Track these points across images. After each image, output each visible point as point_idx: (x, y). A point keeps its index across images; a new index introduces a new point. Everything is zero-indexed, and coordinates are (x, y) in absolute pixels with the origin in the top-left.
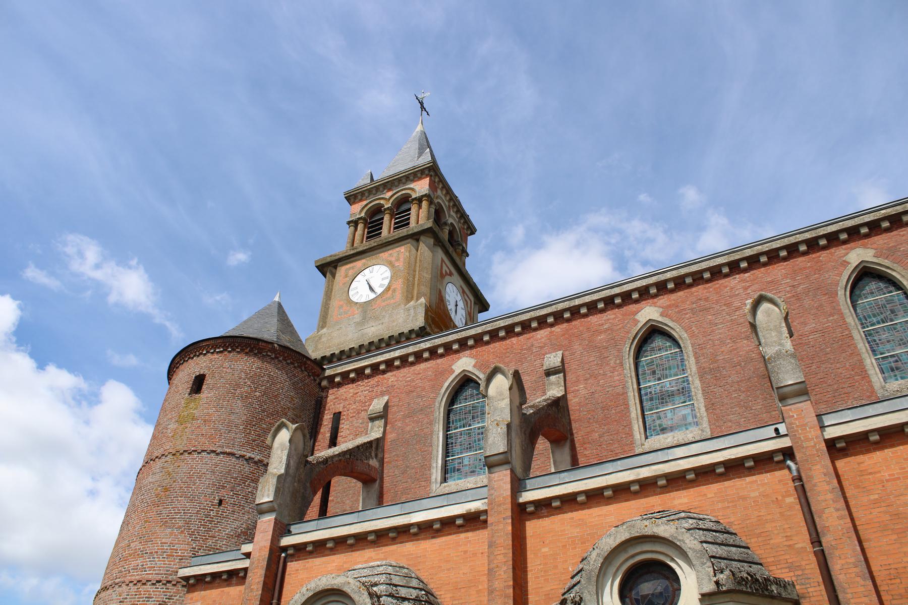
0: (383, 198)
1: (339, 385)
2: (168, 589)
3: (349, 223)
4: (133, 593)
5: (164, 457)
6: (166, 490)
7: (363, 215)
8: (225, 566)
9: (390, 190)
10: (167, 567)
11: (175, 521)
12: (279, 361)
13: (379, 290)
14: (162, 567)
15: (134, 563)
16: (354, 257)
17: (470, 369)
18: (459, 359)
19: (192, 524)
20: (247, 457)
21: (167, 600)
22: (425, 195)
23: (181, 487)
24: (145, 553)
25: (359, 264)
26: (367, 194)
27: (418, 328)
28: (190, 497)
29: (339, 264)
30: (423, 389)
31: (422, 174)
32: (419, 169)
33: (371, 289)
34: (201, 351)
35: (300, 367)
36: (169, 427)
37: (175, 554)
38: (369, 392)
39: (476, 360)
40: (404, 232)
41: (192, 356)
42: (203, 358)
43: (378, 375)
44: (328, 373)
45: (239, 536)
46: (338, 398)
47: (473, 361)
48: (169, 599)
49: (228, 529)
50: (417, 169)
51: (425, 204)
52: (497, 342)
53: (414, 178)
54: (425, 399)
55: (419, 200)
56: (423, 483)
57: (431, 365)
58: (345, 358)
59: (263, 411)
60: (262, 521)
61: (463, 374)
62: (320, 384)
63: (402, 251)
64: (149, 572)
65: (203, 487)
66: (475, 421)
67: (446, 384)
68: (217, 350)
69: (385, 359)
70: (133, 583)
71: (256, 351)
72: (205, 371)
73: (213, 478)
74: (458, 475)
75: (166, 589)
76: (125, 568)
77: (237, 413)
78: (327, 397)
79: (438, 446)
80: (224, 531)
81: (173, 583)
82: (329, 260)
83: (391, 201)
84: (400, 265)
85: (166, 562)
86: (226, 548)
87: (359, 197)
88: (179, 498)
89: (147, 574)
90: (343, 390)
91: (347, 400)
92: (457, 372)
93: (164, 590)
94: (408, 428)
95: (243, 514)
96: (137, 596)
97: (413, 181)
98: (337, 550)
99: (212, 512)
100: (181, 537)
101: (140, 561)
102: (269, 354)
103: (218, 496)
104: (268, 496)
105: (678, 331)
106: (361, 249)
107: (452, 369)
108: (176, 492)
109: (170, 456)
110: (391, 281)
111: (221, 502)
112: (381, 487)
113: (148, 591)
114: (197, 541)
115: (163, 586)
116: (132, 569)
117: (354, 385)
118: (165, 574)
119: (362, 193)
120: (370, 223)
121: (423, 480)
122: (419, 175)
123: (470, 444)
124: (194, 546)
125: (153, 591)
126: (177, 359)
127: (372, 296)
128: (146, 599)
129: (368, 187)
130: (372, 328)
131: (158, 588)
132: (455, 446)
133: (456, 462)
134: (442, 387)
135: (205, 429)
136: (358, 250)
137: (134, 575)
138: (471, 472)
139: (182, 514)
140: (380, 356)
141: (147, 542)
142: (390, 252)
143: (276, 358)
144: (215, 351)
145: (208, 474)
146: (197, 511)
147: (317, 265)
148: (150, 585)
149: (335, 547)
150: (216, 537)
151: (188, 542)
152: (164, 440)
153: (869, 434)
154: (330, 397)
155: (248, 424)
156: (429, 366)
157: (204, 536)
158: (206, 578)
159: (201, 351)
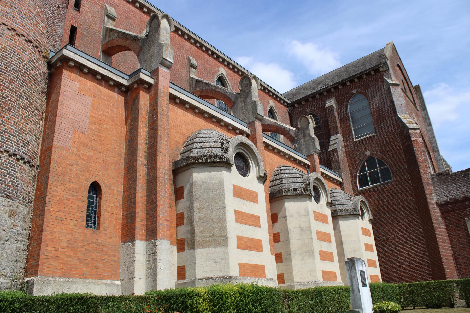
8: (103, 71)
57: (139, 13)
70: (7, 27)
115: (33, 47)
148: (23, 39)
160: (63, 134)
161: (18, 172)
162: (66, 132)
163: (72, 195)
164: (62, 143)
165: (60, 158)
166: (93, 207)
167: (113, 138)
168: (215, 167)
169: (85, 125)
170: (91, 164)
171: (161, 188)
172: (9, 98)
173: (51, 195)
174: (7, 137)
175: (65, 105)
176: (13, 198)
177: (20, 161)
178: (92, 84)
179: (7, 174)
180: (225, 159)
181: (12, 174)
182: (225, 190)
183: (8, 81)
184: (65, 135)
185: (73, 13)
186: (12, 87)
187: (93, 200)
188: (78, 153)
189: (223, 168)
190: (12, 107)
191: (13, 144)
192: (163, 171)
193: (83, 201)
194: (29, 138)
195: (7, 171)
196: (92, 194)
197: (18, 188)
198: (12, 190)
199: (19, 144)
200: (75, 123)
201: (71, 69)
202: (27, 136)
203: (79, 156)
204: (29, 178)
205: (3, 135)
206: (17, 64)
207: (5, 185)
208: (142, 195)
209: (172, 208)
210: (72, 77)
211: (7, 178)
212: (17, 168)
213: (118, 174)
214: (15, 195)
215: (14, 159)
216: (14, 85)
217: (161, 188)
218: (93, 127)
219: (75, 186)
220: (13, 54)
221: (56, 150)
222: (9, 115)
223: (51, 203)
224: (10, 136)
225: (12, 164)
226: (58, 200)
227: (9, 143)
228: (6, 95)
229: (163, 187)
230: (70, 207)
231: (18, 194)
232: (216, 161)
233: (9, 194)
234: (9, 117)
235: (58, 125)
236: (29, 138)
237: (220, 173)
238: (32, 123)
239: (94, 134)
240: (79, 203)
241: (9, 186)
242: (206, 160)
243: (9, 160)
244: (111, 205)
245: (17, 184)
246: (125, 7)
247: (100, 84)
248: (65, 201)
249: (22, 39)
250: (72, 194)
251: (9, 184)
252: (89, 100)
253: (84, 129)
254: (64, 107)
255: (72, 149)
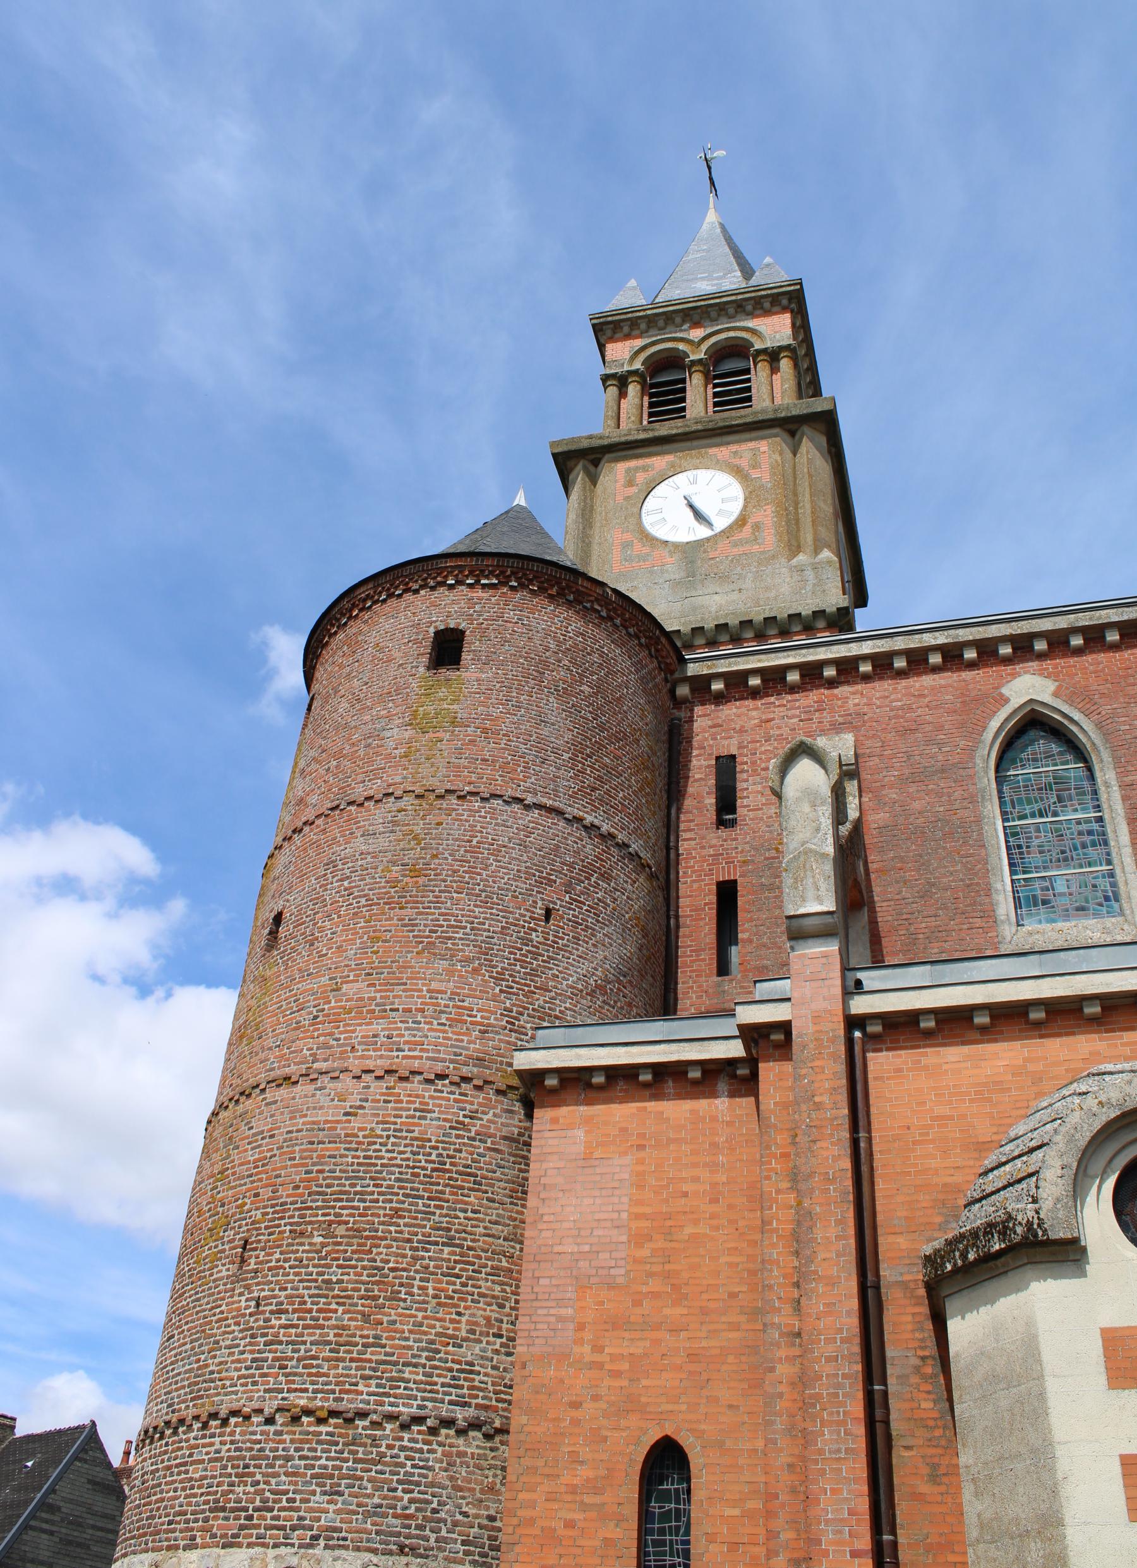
0: (682, 340)
1: (719, 699)
2: (466, 1095)
3: (605, 379)
4: (378, 1097)
5: (392, 799)
6: (415, 872)
7: (638, 365)
8: (649, 1053)
9: (696, 325)
10: (452, 1046)
11: (453, 944)
12: (615, 625)
13: (721, 523)
14: (441, 1045)
15: (361, 1031)
16: (643, 446)
17: (1047, 698)
18: (1014, 675)
19: (496, 956)
20: (587, 822)
21: (467, 1120)
22: (787, 348)
23: (455, 871)
24: (391, 1010)
25: (659, 462)
26: (643, 326)
27: (834, 609)
28: (480, 896)
29: (607, 456)
30: (940, 728)
31: (772, 304)
32: (769, 292)
33: (698, 515)
34: (439, 579)
35: (648, 647)
36: (387, 734)
37: (469, 1019)
38: (801, 720)
39: (1057, 684)
40: (737, 415)
41: (415, 586)
42: (447, 593)
43: (818, 687)
44: (692, 669)
45: (592, 994)
46: (721, 726)
47: (1051, 686)
48: (471, 1118)
49: (572, 976)
50: (763, 293)
51: (785, 364)
52: (1099, 651)
53: (754, 308)
54: (948, 749)
55: (773, 356)
56: (978, 922)
57: (950, 681)
58: (775, 636)
59: (602, 727)
60: (803, 955)
61: (1029, 709)
62: (672, 692)
63: (762, 449)
64: (411, 1054)
65: (506, 877)
66: (1066, 806)
67: (995, 724)
68: (483, 582)
69: (838, 655)
70: (374, 1075)
71: (571, 597)
72: (459, 624)
73: (526, 859)
74: (1045, 913)
75: (461, 1094)
76: (338, 1040)
77: (553, 724)
78: (691, 720)
79: (999, 848)
80: (564, 979)
81: (476, 1082)
82: (585, 444)
83: (704, 347)
84: (763, 475)
85: (450, 1035)
86: (573, 1016)
87: (626, 329)
88: (455, 895)
89: (404, 1057)
90: (730, 711)
91: (746, 731)
92: (1016, 701)
93: (457, 1096)
94: (917, 805)
95: (593, 945)
96: (390, 1105)
97: (752, 315)
98: (1001, 1032)
99: (534, 934)
100: (475, 981)
101: (380, 1027)
102: (597, 607)
103: (543, 899)
104: (819, 900)
105: (1087, 730)
106: (666, 433)
107: (1001, 695)
108: (445, 881)
109: (408, 799)
110: (745, 507)
111: (548, 913)
112: (873, 923)
113: (417, 1096)
114: (514, 994)
115: (453, 1088)
116: (360, 1043)
117: (759, 703)
118: (452, 1061)
119: (634, 323)
120: (652, 386)
121: (975, 914)
122: (767, 305)
123: (1063, 852)
124: (508, 1005)
125: (431, 1097)
126: (362, 593)
127: (703, 532)
128: (418, 1114)
129: (649, 312)
130: (716, 597)
131: (442, 1092)
132: (1029, 853)
133: (1037, 885)
134: (984, 728)
135: (487, 749)
136: (657, 434)
137: (370, 1057)
138: (1078, 909)
139: (468, 930)
140: (824, 649)
141: (392, 984)
142: (734, 448)
143: (610, 618)
144: (478, 582)
145: (513, 848)
146: (503, 927)
147: (556, 451)
148: (420, 1082)
149: (992, 1024)
150: (550, 991)
151: (494, 995)
152: (379, 762)
153: (868, 1022)
154: (700, 724)
155: (577, 750)
156: (943, 682)
157: (526, 985)
158: (592, 1077)
159: (439, 579)
160: (545, 1312)
161: (438, 1465)
162: (553, 1304)
163: (585, 1508)
164: (543, 1341)
165: (537, 1392)
166: (678, 1528)
167: (723, 1260)
168: (1006, 1272)
169: (614, 1255)
170: (644, 1382)
171: (822, 1421)
172: (391, 1265)
173: (515, 1521)
174: (394, 1374)
175: (546, 1218)
176: (422, 1551)
177: (443, 1431)
178: (632, 1107)
179: (399, 1482)
180: (1019, 1230)
181: (416, 1478)
182: (1047, 1372)
183: (386, 1219)
184: (552, 1311)
185: (714, 842)
186: (396, 1232)
187: (678, 1502)
188: (597, 1357)
189: (1029, 1271)
190: (401, 1285)
191: (412, 1390)
192: (830, 1350)
193: (620, 1520)
194: (469, 1352)
195: (399, 1474)
196: (672, 1484)
197: (442, 1515)
198: (418, 1527)
199: (436, 1384)
200: (581, 1264)
201: (555, 1097)
202: (463, 1350)
203: (600, 1366)
204: (487, 1472)
205: (379, 1374)
206: (408, 1159)
207: (395, 1516)
208: (790, 1460)
209: (945, 1480)
210: (561, 1121)
211: (399, 1493)
212: (431, 1456)
213: (750, 1387)
214: (432, 1540)
215: (419, 1432)
216: (401, 1221)
217: (822, 1421)
218: (645, 1252)
219: (591, 1474)
220: (395, 1137)
221: (526, 1372)
222: (393, 1312)
223: (517, 1549)
224: (400, 1371)
225: (412, 1448)
226: (538, 1532)
227: (401, 1391)
228: (382, 1261)
229: (831, 1414)
230: (578, 1551)
231: (444, 1533)
232: (993, 1250)
233: (407, 1542)
234: (394, 1318)
235: (529, 1289)
236: (469, 1352)
237: (1022, 1296)
238: (481, 1305)
239: (650, 1275)
240: (612, 1531)
241: (407, 1517)
242: (964, 1256)
243: (401, 1439)
244: (729, 1512)
245: (435, 1505)
246: (892, 697)
247: (657, 1097)
248: (561, 1531)
249: (416, 1084)
250: (582, 1502)
251: (408, 1512)
252: (621, 1166)
253: (613, 1271)
254: (544, 1226)
255: (577, 1349)
